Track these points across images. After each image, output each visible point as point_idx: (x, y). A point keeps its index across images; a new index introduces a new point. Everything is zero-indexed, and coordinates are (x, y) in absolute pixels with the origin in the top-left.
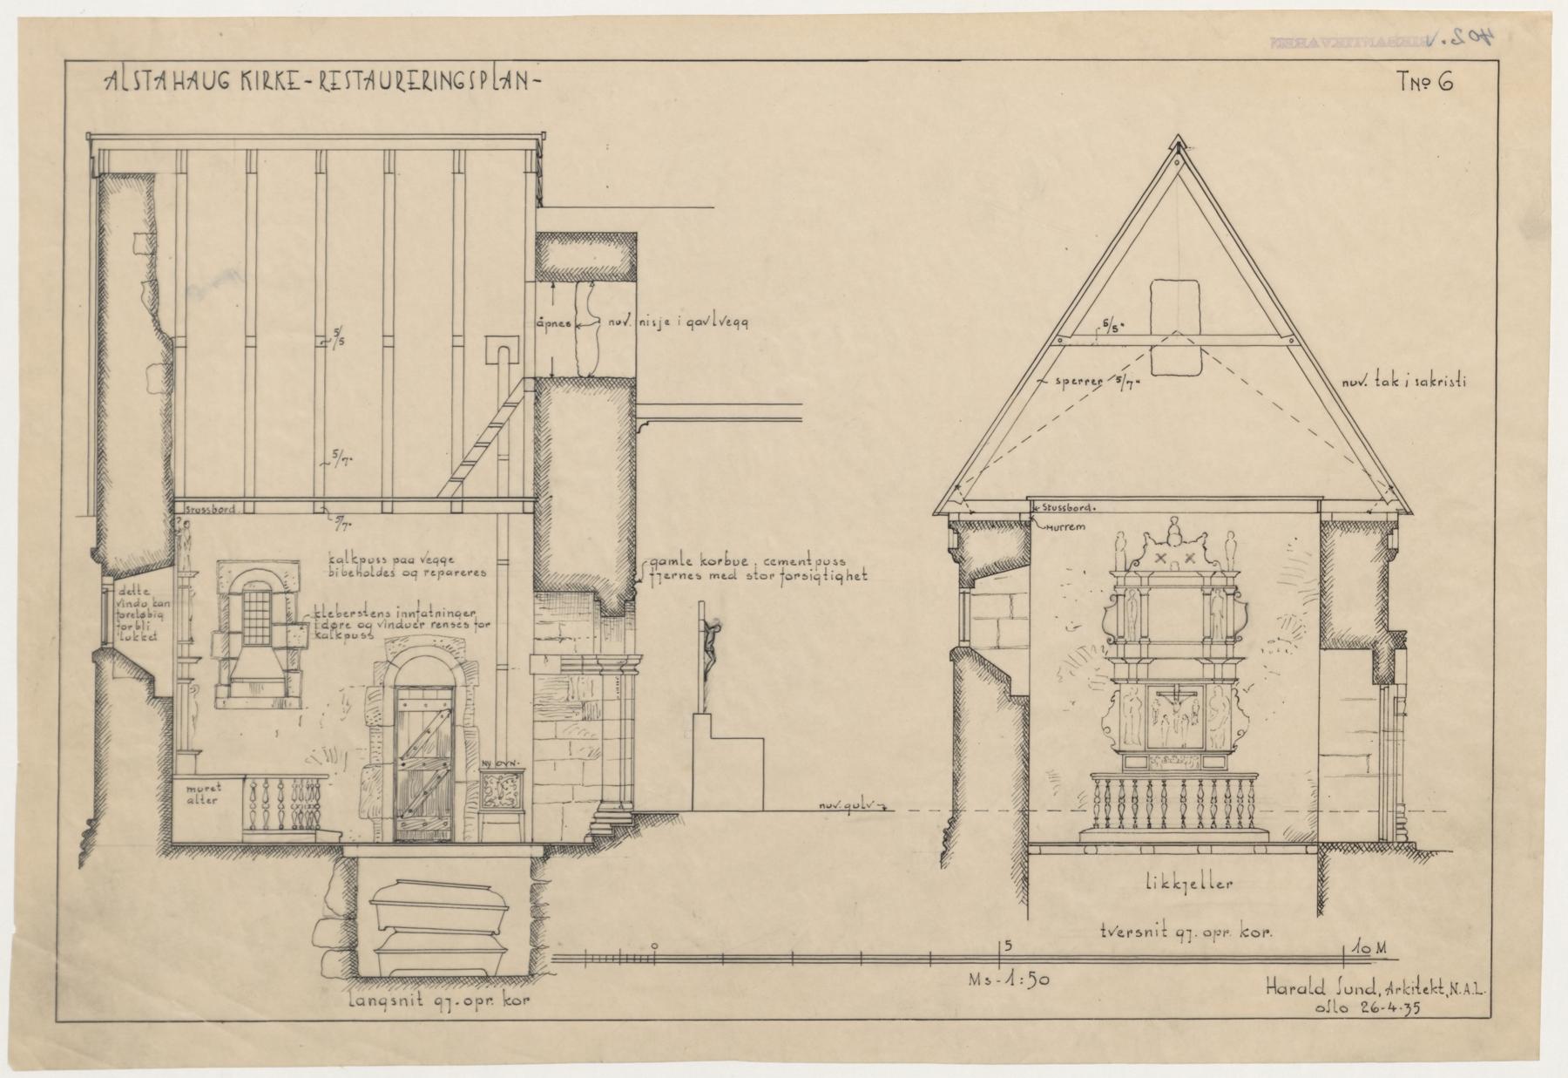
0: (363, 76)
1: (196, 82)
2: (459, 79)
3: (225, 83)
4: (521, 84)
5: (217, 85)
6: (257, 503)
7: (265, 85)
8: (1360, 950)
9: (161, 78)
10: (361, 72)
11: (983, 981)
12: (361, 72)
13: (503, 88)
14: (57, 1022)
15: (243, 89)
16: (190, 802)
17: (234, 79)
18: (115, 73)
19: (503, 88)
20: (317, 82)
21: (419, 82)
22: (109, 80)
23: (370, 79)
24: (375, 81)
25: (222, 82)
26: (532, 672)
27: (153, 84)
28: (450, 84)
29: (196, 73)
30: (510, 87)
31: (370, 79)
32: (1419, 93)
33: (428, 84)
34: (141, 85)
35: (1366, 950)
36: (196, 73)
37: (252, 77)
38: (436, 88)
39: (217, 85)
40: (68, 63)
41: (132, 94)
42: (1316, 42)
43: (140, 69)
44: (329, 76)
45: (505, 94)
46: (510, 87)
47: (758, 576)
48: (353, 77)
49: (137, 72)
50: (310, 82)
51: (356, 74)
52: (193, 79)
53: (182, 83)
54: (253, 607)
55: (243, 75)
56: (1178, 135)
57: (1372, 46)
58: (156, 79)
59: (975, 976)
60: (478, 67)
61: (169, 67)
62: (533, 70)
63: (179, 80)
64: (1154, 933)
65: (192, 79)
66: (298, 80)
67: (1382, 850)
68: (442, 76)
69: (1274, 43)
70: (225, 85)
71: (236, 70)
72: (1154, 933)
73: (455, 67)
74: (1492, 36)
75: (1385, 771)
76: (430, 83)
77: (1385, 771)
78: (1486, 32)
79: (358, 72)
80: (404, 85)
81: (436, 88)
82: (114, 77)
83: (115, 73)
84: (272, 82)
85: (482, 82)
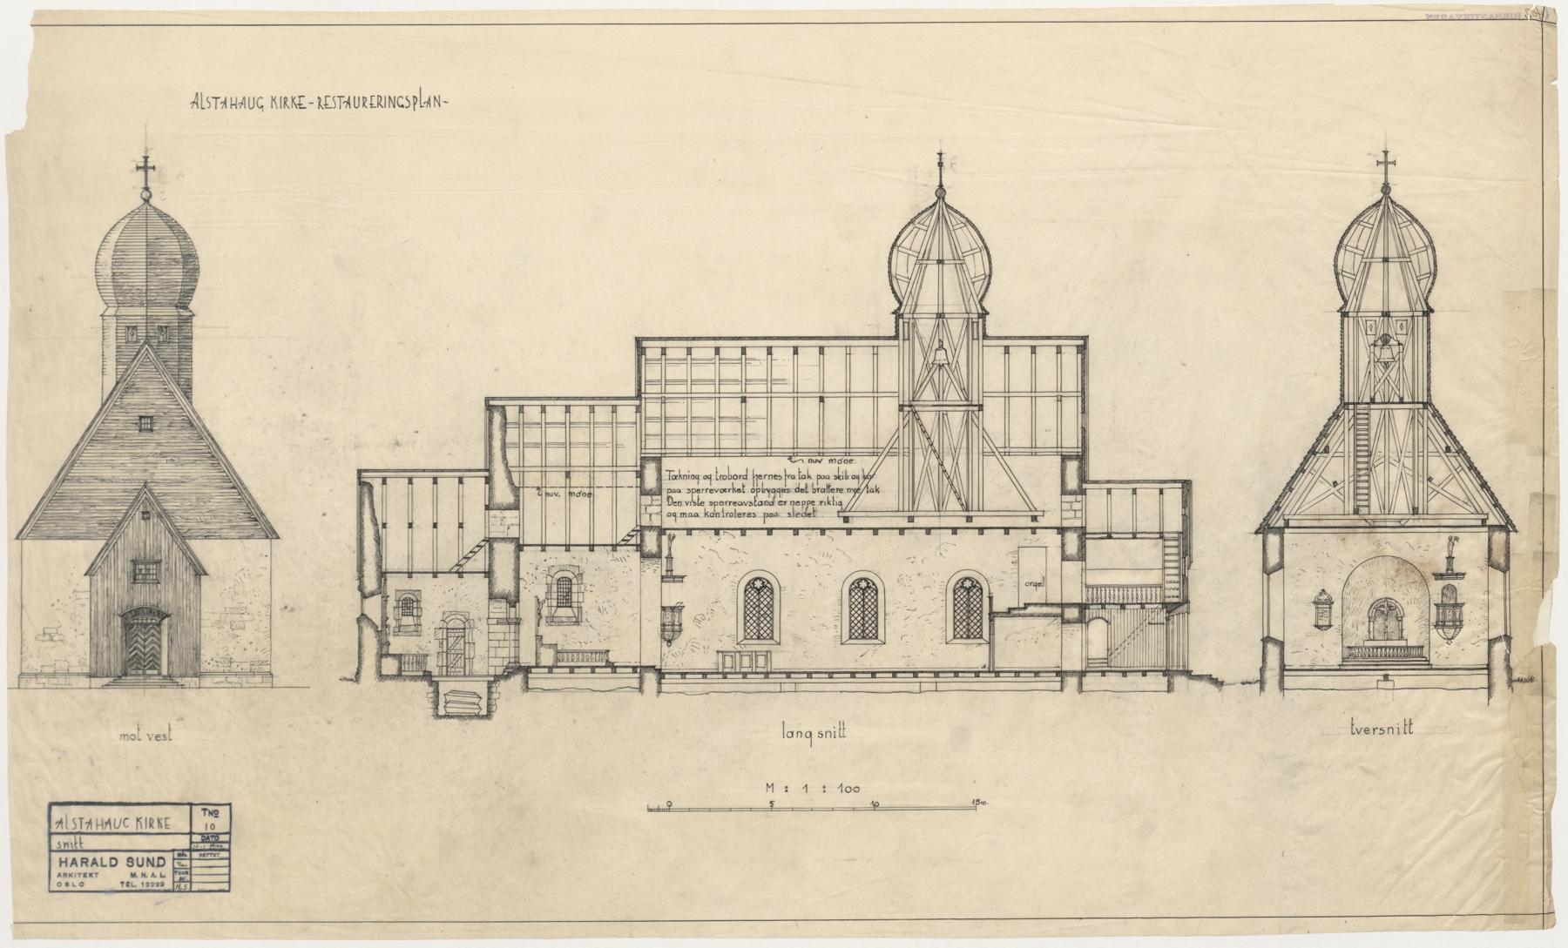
5: (256, 106)
10: (1262, 688)
12: (1262, 688)
14: (50, 891)
15: (272, 107)
20: (316, 104)
21: (375, 102)
27: (219, 106)
29: (244, 98)
36: (244, 98)
39: (256, 106)
47: (756, 503)
54: (870, 622)
63: (234, 103)
64: (1396, 731)
67: (1555, 498)
68: (390, 97)
72: (1396, 731)
75: (906, 458)
77: (906, 458)
80: (367, 104)
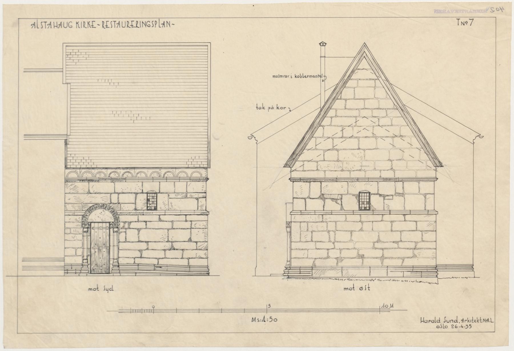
0: (47, 24)
1: (35, 25)
2: (148, 23)
3: (149, 25)
4: (168, 25)
6: (403, 209)
7: (128, 26)
8: (385, 306)
9: (33, 24)
10: (46, 22)
11: (257, 320)
12: (46, 22)
13: (162, 27)
16: (253, 318)
17: (74, 25)
18: (35, 23)
19: (162, 27)
20: (101, 26)
21: (135, 25)
22: (49, 25)
23: (119, 24)
24: (120, 25)
25: (148, 25)
26: (474, 272)
27: (47, 26)
28: (145, 25)
30: (165, 27)
31: (119, 24)
32: (120, 28)
33: (138, 26)
34: (112, 26)
35: (387, 306)
37: (80, 23)
38: (140, 27)
40: (20, 19)
41: (40, 29)
42: (449, 11)
43: (112, 21)
44: (130, 22)
45: (163, 29)
46: (165, 27)
48: (44, 24)
49: (42, 22)
50: (98, 25)
51: (45, 23)
52: (60, 25)
53: (57, 26)
55: (77, 23)
56: (364, 43)
57: (468, 13)
58: (48, 25)
59: (254, 319)
60: (154, 20)
61: (52, 21)
62: (172, 21)
65: (60, 25)
66: (95, 24)
68: (143, 22)
69: (435, 11)
70: (71, 27)
71: (74, 21)
73: (147, 20)
74: (503, 9)
76: (138, 25)
78: (502, 8)
79: (45, 22)
81: (140, 27)
82: (34, 24)
83: (35, 23)
84: (86, 25)
85: (156, 25)
